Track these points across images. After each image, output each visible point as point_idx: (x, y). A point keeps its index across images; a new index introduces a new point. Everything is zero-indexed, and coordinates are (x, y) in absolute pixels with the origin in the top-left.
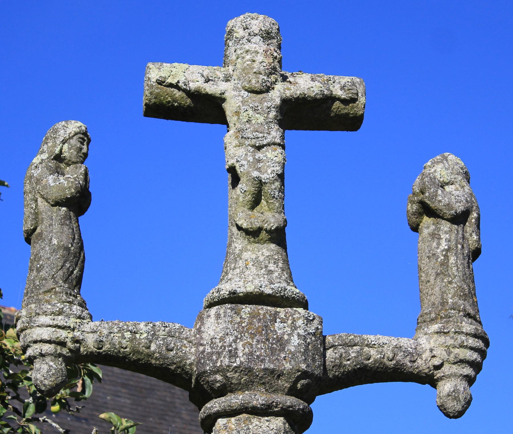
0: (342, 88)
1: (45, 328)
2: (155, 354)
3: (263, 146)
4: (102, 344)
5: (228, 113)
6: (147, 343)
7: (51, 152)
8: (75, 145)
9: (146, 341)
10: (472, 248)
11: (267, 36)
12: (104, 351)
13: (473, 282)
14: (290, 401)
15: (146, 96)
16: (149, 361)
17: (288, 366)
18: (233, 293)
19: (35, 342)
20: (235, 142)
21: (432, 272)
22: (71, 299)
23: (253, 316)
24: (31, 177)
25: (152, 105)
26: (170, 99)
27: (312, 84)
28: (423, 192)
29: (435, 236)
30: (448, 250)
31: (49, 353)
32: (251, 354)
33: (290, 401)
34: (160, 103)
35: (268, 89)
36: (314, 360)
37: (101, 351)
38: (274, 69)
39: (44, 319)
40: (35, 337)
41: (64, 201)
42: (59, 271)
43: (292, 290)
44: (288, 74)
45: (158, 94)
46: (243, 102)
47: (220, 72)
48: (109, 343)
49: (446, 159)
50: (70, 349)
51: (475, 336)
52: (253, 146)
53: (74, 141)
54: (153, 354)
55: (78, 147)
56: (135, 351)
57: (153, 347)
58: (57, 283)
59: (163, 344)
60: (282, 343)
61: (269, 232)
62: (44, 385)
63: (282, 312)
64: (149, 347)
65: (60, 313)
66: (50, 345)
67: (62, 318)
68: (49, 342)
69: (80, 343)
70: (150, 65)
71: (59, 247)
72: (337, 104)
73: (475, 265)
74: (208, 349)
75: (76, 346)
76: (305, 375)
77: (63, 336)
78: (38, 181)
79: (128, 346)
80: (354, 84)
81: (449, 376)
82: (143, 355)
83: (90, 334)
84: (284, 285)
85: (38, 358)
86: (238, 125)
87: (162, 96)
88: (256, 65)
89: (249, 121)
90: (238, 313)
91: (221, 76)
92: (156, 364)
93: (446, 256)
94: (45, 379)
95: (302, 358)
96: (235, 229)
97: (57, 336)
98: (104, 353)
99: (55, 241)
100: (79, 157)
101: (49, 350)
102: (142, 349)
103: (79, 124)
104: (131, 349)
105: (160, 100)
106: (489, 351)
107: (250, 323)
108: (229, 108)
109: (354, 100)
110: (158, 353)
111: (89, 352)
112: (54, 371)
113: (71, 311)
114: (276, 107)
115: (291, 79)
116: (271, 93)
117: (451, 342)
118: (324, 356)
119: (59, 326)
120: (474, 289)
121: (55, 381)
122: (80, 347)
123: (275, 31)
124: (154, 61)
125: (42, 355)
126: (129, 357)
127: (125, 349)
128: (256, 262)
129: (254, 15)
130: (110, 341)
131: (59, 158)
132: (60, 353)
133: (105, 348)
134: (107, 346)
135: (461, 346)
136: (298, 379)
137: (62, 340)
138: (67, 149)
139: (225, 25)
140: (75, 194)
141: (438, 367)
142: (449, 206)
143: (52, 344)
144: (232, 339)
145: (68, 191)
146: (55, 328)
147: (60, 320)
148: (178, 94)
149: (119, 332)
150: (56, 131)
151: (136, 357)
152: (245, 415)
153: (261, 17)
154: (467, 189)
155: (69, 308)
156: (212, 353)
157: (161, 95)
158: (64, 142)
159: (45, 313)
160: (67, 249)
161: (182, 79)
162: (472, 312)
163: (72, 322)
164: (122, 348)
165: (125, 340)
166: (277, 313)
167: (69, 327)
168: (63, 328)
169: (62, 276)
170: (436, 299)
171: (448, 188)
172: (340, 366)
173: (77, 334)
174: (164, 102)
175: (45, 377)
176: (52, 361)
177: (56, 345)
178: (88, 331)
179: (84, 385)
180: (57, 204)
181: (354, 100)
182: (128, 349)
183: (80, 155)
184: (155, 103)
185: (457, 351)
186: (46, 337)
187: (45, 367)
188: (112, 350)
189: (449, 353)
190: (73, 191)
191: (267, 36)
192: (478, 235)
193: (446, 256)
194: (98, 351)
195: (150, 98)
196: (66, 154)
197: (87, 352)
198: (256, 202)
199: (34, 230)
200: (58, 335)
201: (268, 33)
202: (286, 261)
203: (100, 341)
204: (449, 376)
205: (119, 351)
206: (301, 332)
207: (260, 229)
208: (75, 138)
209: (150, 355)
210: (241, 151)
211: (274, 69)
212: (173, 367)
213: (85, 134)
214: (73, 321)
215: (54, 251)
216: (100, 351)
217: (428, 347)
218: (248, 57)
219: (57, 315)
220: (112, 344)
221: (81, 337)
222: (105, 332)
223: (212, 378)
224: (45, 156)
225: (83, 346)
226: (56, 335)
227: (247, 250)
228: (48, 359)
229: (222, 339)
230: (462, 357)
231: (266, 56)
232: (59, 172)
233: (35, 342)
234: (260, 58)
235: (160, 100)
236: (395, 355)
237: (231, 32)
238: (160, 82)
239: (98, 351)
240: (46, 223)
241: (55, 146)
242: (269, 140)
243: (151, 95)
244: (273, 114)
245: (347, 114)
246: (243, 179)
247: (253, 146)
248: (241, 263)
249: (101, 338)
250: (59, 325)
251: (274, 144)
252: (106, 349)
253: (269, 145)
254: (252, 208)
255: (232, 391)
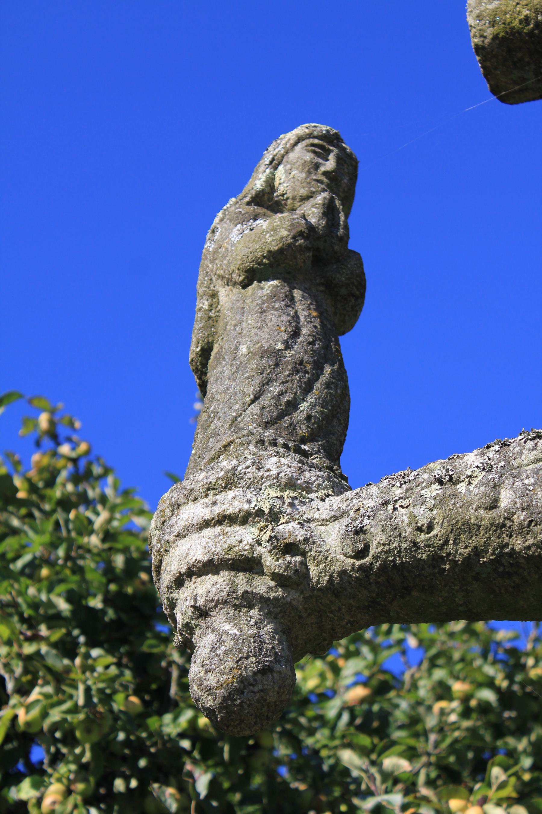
1: (196, 536)
2: (515, 516)
4: (364, 540)
6: (485, 493)
8: (299, 158)
9: (483, 489)
12: (376, 558)
16: (507, 545)
25: (490, 44)
26: (528, 12)
31: (216, 598)
34: (507, 33)
37: (367, 560)
41: (265, 264)
42: (249, 405)
45: (495, 12)
48: (380, 528)
50: (275, 576)
54: (509, 519)
55: (306, 162)
59: (533, 485)
62: (209, 690)
64: (494, 505)
66: (216, 576)
67: (238, 494)
69: (304, 554)
75: (290, 563)
77: (245, 543)
79: (436, 521)
82: (482, 532)
83: (331, 526)
85: (196, 626)
87: (506, 13)
92: (529, 547)
94: (207, 671)
97: (227, 546)
98: (376, 566)
100: (313, 183)
101: (213, 590)
104: (446, 525)
105: (504, 24)
110: (523, 510)
111: (335, 575)
112: (230, 643)
113: (259, 469)
119: (229, 515)
121: (235, 671)
122: (304, 564)
126: (449, 554)
127: (428, 533)
130: (383, 523)
132: (246, 592)
133: (375, 547)
134: (379, 538)
137: (245, 553)
138: (284, 176)
140: (290, 241)
143: (222, 573)
145: (271, 236)
146: (220, 527)
149: (409, 493)
151: (466, 547)
155: (253, 464)
157: (502, 11)
164: (419, 529)
165: (423, 507)
167: (260, 513)
169: (256, 414)
174: (516, 23)
175: (208, 667)
176: (228, 621)
177: (232, 573)
178: (323, 517)
182: (436, 531)
183: (314, 178)
184: (495, 37)
188: (395, 544)
190: (284, 233)
194: (359, 563)
195: (480, 30)
197: (331, 576)
200: (232, 541)
203: (357, 533)
205: (415, 544)
208: (300, 146)
214: (270, 496)
216: (366, 560)
219: (222, 491)
220: (388, 529)
221: (300, 534)
225: (314, 559)
226: (225, 542)
235: (504, 24)
239: (359, 563)
243: (480, 20)
249: (358, 522)
250: (228, 512)
252: (379, 550)
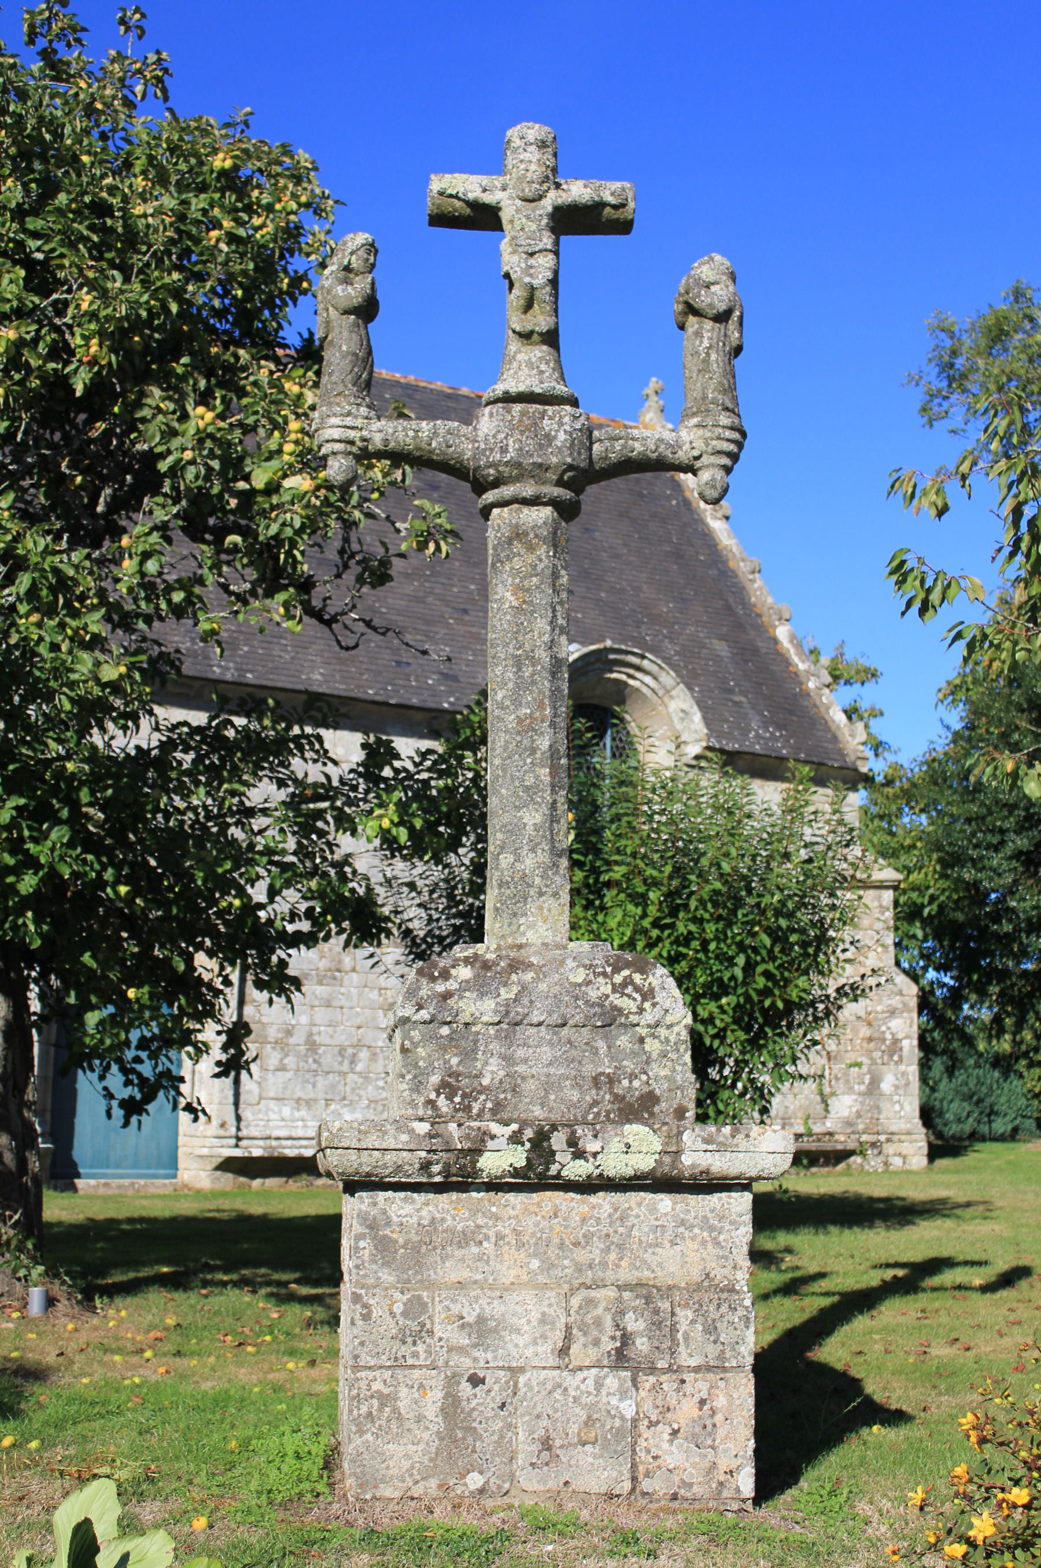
0: (612, 194)
3: (535, 253)
5: (504, 222)
7: (340, 264)
10: (734, 345)
11: (542, 145)
13: (734, 377)
14: (557, 492)
15: (429, 207)
17: (554, 460)
18: (507, 393)
19: (327, 441)
20: (510, 250)
21: (695, 369)
22: (359, 401)
23: (523, 414)
24: (323, 287)
27: (584, 191)
28: (687, 293)
29: (698, 334)
30: (710, 347)
32: (521, 449)
33: (557, 492)
35: (540, 198)
36: (579, 453)
38: (547, 177)
39: (334, 421)
40: (327, 437)
43: (561, 389)
44: (562, 181)
46: (518, 211)
47: (498, 181)
49: (712, 259)
51: (732, 428)
52: (526, 253)
53: (361, 253)
56: (419, 449)
57: (434, 444)
58: (346, 386)
60: (549, 438)
61: (541, 334)
63: (550, 410)
65: (349, 414)
68: (340, 441)
70: (433, 177)
71: (348, 353)
72: (608, 209)
73: (736, 362)
74: (483, 446)
76: (570, 467)
78: (329, 291)
80: (623, 189)
81: (707, 466)
84: (554, 384)
86: (513, 233)
88: (529, 175)
89: (522, 229)
90: (509, 412)
91: (499, 185)
93: (708, 354)
95: (567, 452)
96: (510, 332)
99: (344, 348)
102: (424, 446)
103: (367, 235)
106: (746, 444)
107: (520, 421)
108: (505, 216)
109: (623, 206)
114: (548, 215)
115: (564, 187)
116: (544, 202)
117: (708, 434)
118: (590, 449)
120: (735, 383)
123: (550, 139)
124: (437, 172)
125: (334, 453)
128: (530, 364)
129: (530, 124)
131: (347, 269)
135: (719, 438)
136: (564, 472)
139: (504, 135)
141: (697, 458)
142: (711, 305)
144: (503, 436)
147: (349, 421)
148: (458, 204)
150: (345, 243)
152: (516, 506)
153: (537, 126)
154: (731, 289)
156: (485, 450)
158: (352, 253)
159: (335, 415)
160: (355, 355)
161: (462, 190)
162: (730, 406)
163: (359, 423)
166: (545, 411)
168: (352, 428)
170: (697, 394)
171: (713, 288)
172: (606, 458)
173: (365, 433)
179: (404, 474)
180: (346, 312)
181: (623, 206)
185: (714, 443)
186: (336, 437)
187: (337, 464)
189: (707, 445)
191: (542, 145)
192: (741, 333)
193: (708, 354)
196: (354, 265)
198: (529, 306)
199: (326, 337)
201: (543, 142)
202: (558, 362)
204: (707, 466)
206: (567, 428)
207: (532, 332)
209: (431, 452)
210: (515, 258)
211: (547, 177)
212: (452, 462)
213: (372, 245)
215: (344, 357)
217: (688, 439)
218: (522, 166)
222: (391, 431)
223: (485, 472)
224: (334, 268)
227: (520, 352)
228: (339, 457)
229: (494, 436)
230: (719, 448)
231: (539, 165)
232: (347, 281)
233: (327, 441)
234: (533, 167)
236: (657, 447)
237: (509, 142)
238: (441, 194)
240: (337, 330)
241: (343, 258)
242: (541, 246)
244: (545, 221)
245: (618, 219)
246: (517, 285)
247: (526, 253)
248: (515, 364)
251: (546, 250)
253: (540, 251)
254: (525, 312)
255: (504, 484)
